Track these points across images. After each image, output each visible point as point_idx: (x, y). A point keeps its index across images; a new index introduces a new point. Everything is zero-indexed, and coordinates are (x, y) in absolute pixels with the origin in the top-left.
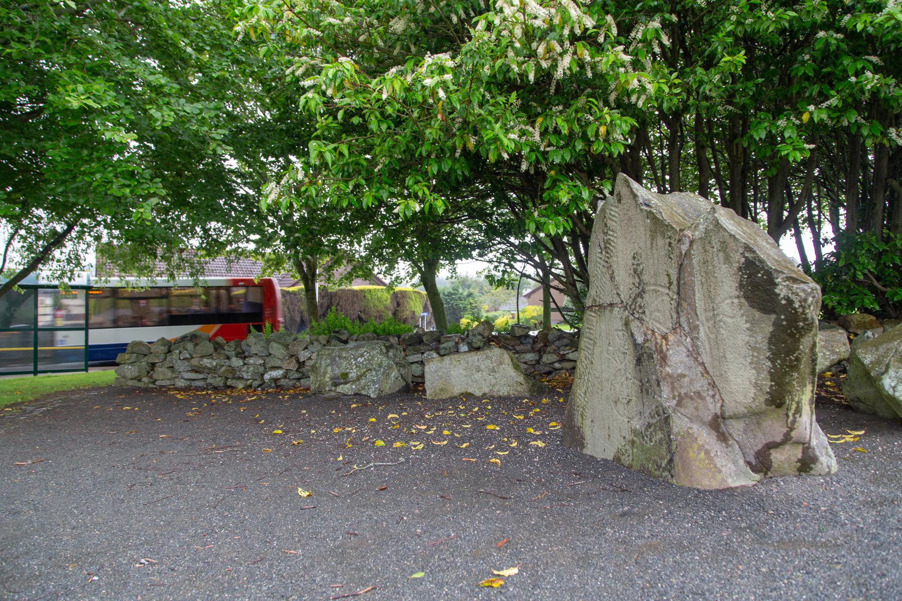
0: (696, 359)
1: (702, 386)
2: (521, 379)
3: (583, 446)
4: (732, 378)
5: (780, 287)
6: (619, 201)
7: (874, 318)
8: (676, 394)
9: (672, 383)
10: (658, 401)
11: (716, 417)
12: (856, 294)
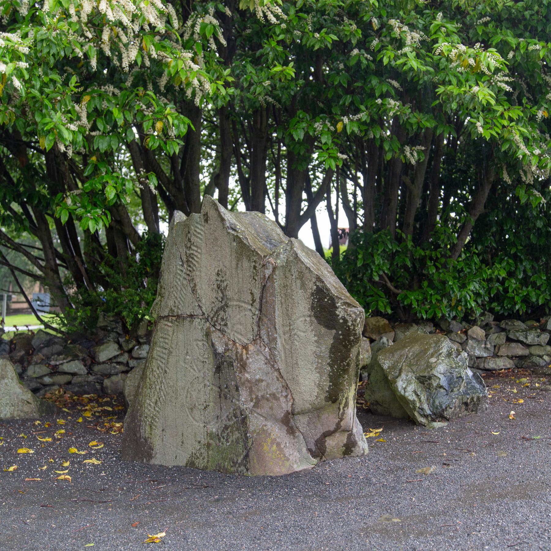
0: (273, 366)
1: (277, 389)
2: (28, 396)
3: (150, 456)
4: (302, 381)
5: (340, 310)
6: (206, 221)
7: (386, 321)
8: (254, 396)
9: (251, 388)
10: (236, 405)
11: (288, 413)
12: (372, 296)
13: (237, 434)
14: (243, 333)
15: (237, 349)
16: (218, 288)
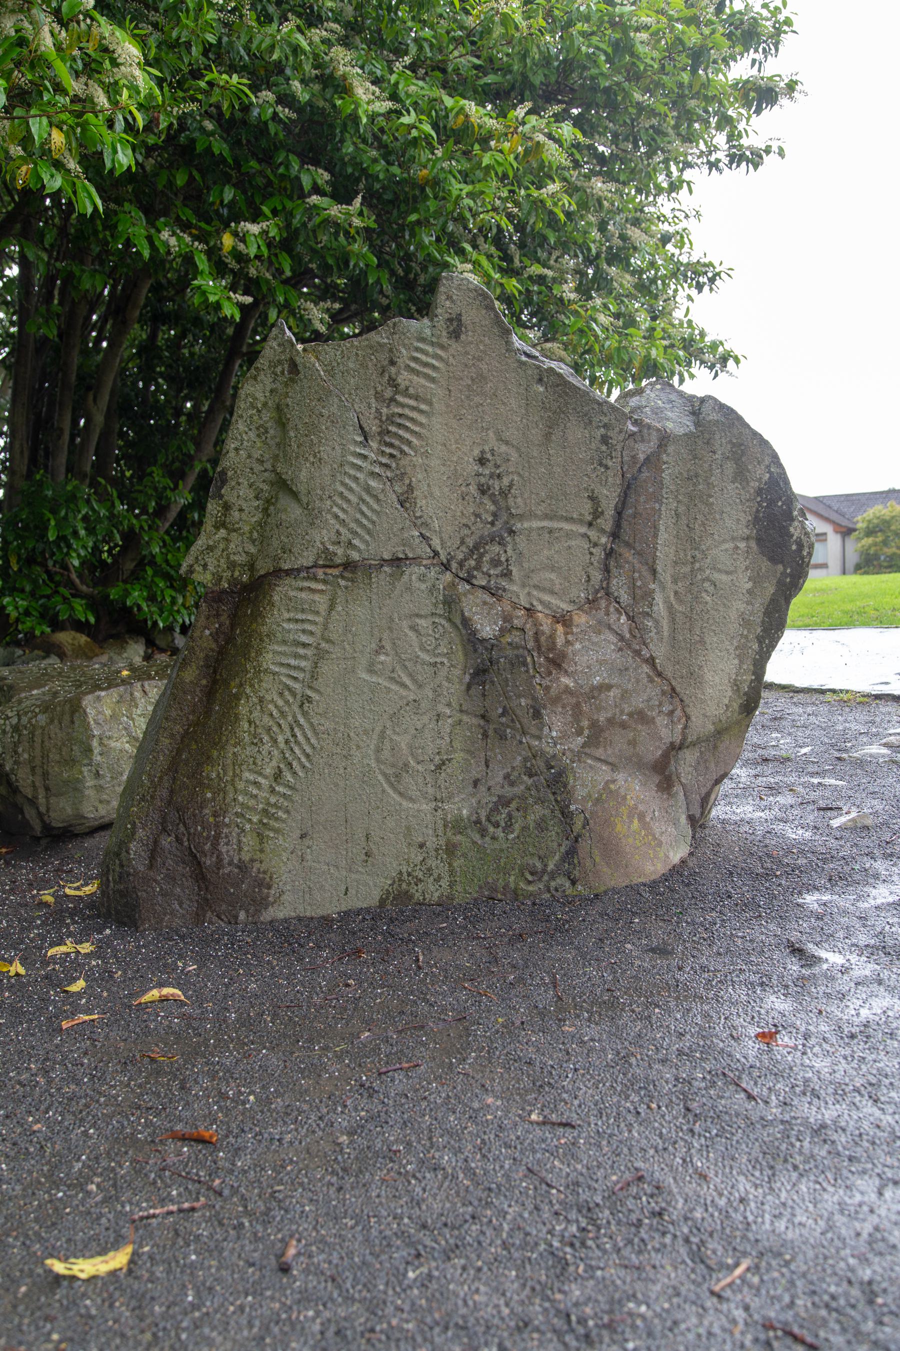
0: (638, 653)
4: (709, 676)
6: (456, 334)
8: (585, 723)
13: (538, 811)
14: (557, 588)
15: (537, 624)
16: (483, 492)
